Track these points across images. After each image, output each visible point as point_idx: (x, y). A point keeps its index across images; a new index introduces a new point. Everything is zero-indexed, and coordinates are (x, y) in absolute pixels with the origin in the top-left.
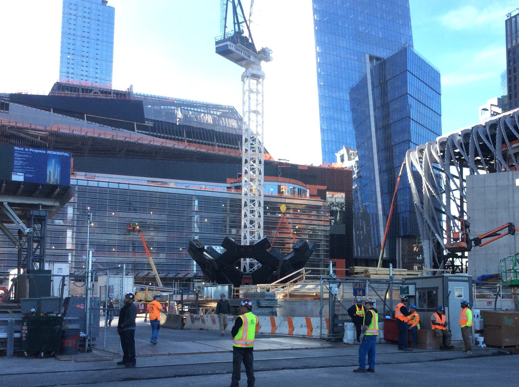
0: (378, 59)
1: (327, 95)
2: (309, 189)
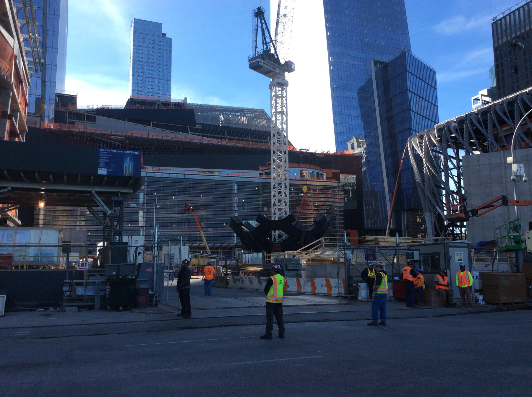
0: (381, 63)
2: (325, 172)
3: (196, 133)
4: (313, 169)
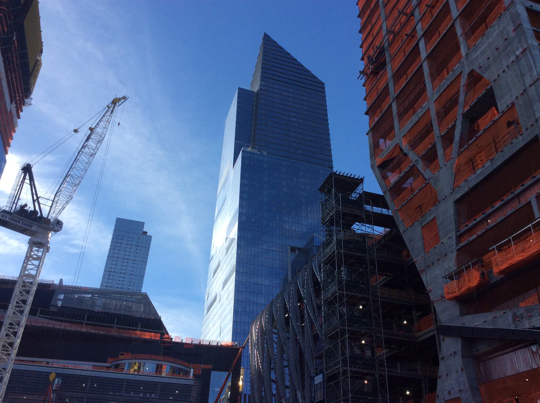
0: (299, 249)
3: (46, 316)
4: (171, 362)
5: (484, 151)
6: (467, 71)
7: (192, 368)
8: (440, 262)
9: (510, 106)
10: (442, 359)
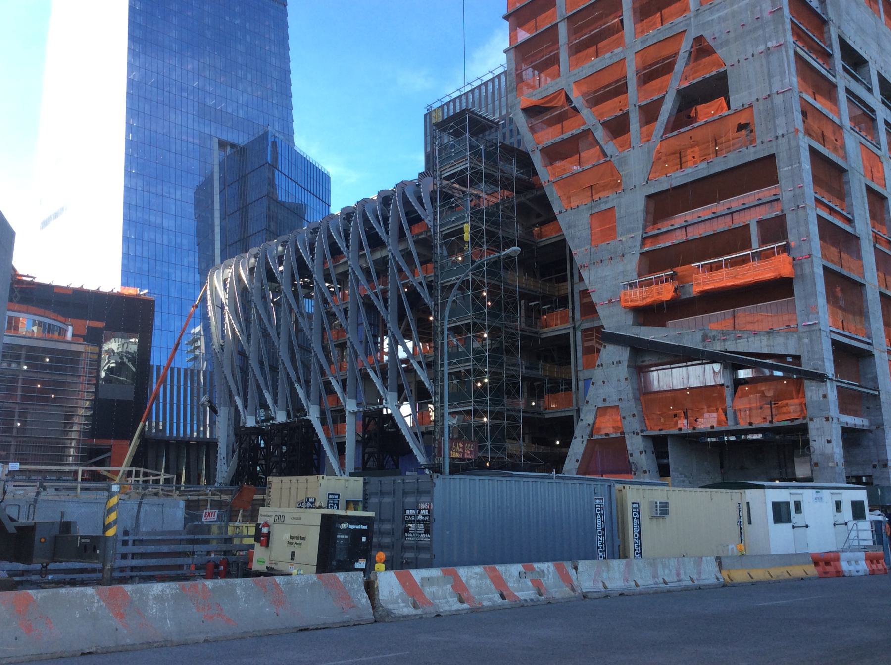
0: (233, 146)
1: (140, 188)
2: (72, 325)
5: (698, 146)
6: (693, 33)
7: (70, 325)
8: (613, 262)
9: (746, 106)
10: (599, 366)
